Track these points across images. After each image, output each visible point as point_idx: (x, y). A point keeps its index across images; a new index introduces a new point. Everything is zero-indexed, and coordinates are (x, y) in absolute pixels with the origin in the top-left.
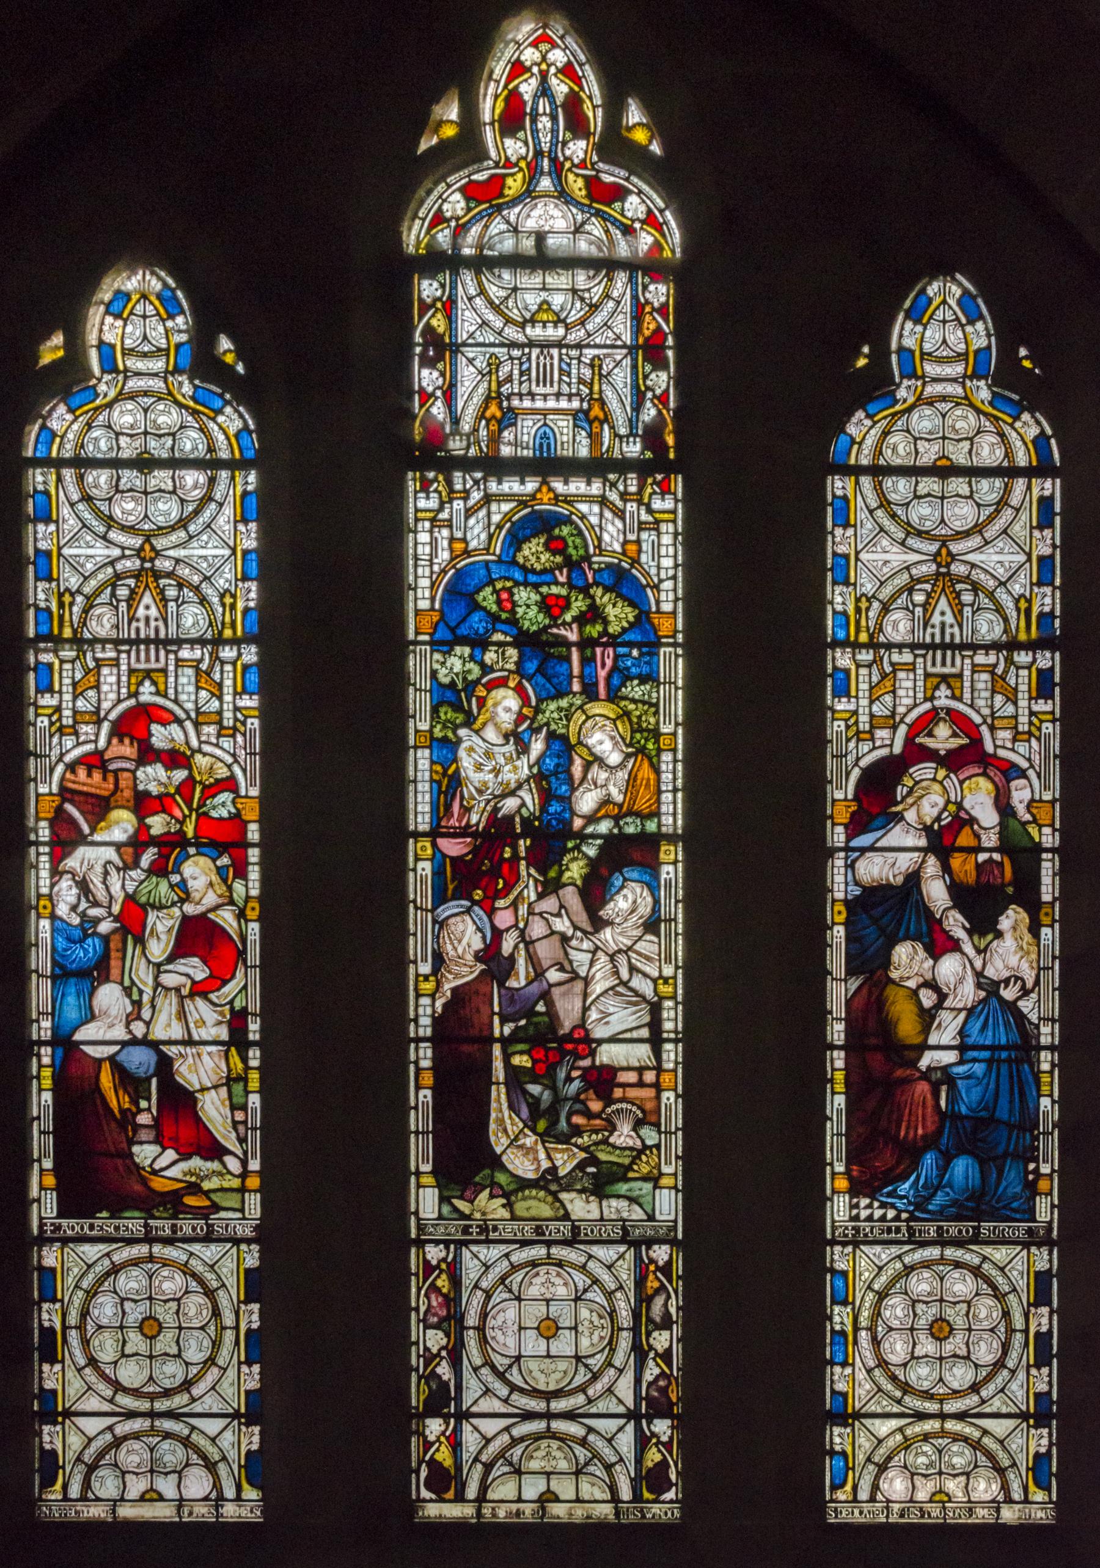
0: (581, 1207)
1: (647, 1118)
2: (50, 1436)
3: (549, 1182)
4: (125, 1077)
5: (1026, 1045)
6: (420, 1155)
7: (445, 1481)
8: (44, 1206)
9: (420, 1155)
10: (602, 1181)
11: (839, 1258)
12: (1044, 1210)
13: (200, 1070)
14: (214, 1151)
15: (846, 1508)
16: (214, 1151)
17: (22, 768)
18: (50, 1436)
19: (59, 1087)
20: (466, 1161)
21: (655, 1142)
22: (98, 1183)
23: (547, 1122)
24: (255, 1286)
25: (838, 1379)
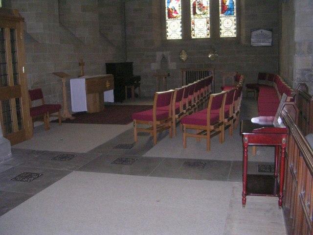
0: (202, 16)
1: (207, 10)
2: (221, 31)
3: (200, 14)
4: (173, 10)
5: (233, 3)
6: (192, 13)
7: (194, 35)
8: (167, 18)
9: (192, 13)
10: (204, 14)
11: (221, 19)
12: (235, 14)
13: (177, 8)
14: (177, 13)
15: (222, 36)
16: (177, 13)
17: (219, 32)
18: (221, 31)
19: (168, 10)
20: (195, 13)
21: (208, 11)
22: (170, 16)
23: (200, 10)
24: (181, 23)
25: (221, 27)
